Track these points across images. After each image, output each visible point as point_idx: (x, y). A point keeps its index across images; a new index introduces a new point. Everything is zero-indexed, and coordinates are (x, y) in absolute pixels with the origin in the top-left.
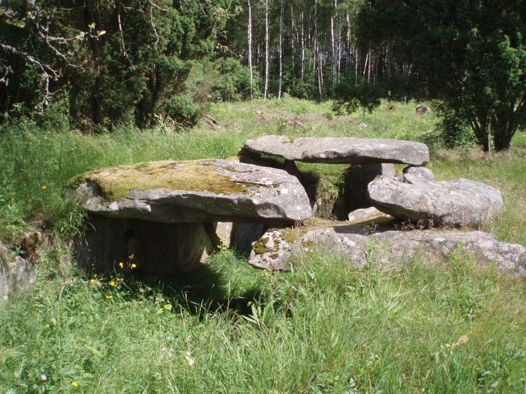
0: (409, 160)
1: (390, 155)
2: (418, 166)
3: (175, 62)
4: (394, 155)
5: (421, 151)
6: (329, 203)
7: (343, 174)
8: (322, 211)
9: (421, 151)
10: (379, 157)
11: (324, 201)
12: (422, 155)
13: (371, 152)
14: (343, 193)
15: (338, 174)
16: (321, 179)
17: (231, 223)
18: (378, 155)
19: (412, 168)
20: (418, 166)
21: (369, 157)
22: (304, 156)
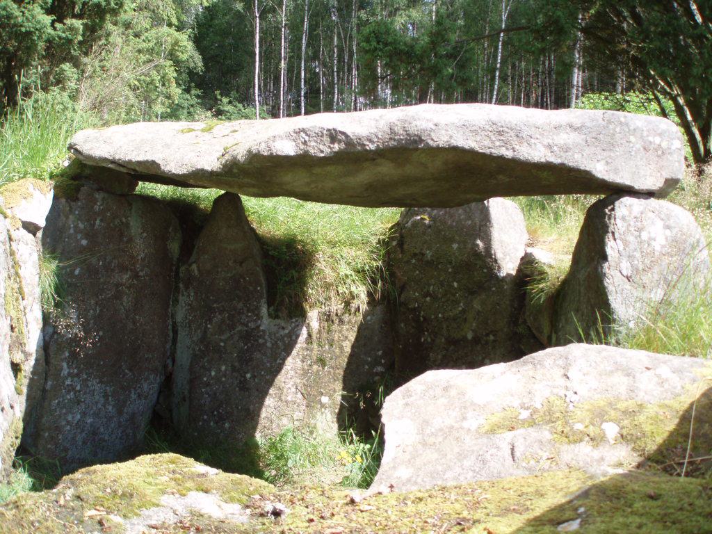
0: (616, 171)
1: (550, 147)
2: (649, 194)
3: (33, 17)
4: (566, 149)
5: (657, 140)
6: (341, 321)
7: (379, 242)
8: (319, 345)
9: (657, 140)
10: (509, 154)
11: (327, 318)
12: (661, 153)
13: (475, 132)
14: (378, 296)
15: (365, 243)
16: (320, 256)
17: (503, 274)
18: (506, 144)
19: (627, 200)
20: (649, 194)
21: (472, 152)
22: (227, 157)
